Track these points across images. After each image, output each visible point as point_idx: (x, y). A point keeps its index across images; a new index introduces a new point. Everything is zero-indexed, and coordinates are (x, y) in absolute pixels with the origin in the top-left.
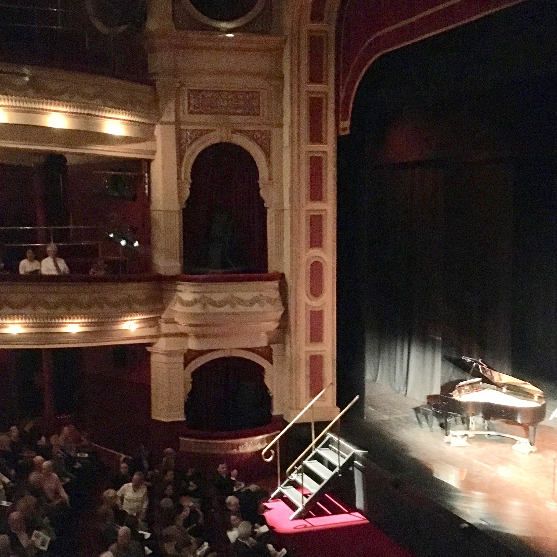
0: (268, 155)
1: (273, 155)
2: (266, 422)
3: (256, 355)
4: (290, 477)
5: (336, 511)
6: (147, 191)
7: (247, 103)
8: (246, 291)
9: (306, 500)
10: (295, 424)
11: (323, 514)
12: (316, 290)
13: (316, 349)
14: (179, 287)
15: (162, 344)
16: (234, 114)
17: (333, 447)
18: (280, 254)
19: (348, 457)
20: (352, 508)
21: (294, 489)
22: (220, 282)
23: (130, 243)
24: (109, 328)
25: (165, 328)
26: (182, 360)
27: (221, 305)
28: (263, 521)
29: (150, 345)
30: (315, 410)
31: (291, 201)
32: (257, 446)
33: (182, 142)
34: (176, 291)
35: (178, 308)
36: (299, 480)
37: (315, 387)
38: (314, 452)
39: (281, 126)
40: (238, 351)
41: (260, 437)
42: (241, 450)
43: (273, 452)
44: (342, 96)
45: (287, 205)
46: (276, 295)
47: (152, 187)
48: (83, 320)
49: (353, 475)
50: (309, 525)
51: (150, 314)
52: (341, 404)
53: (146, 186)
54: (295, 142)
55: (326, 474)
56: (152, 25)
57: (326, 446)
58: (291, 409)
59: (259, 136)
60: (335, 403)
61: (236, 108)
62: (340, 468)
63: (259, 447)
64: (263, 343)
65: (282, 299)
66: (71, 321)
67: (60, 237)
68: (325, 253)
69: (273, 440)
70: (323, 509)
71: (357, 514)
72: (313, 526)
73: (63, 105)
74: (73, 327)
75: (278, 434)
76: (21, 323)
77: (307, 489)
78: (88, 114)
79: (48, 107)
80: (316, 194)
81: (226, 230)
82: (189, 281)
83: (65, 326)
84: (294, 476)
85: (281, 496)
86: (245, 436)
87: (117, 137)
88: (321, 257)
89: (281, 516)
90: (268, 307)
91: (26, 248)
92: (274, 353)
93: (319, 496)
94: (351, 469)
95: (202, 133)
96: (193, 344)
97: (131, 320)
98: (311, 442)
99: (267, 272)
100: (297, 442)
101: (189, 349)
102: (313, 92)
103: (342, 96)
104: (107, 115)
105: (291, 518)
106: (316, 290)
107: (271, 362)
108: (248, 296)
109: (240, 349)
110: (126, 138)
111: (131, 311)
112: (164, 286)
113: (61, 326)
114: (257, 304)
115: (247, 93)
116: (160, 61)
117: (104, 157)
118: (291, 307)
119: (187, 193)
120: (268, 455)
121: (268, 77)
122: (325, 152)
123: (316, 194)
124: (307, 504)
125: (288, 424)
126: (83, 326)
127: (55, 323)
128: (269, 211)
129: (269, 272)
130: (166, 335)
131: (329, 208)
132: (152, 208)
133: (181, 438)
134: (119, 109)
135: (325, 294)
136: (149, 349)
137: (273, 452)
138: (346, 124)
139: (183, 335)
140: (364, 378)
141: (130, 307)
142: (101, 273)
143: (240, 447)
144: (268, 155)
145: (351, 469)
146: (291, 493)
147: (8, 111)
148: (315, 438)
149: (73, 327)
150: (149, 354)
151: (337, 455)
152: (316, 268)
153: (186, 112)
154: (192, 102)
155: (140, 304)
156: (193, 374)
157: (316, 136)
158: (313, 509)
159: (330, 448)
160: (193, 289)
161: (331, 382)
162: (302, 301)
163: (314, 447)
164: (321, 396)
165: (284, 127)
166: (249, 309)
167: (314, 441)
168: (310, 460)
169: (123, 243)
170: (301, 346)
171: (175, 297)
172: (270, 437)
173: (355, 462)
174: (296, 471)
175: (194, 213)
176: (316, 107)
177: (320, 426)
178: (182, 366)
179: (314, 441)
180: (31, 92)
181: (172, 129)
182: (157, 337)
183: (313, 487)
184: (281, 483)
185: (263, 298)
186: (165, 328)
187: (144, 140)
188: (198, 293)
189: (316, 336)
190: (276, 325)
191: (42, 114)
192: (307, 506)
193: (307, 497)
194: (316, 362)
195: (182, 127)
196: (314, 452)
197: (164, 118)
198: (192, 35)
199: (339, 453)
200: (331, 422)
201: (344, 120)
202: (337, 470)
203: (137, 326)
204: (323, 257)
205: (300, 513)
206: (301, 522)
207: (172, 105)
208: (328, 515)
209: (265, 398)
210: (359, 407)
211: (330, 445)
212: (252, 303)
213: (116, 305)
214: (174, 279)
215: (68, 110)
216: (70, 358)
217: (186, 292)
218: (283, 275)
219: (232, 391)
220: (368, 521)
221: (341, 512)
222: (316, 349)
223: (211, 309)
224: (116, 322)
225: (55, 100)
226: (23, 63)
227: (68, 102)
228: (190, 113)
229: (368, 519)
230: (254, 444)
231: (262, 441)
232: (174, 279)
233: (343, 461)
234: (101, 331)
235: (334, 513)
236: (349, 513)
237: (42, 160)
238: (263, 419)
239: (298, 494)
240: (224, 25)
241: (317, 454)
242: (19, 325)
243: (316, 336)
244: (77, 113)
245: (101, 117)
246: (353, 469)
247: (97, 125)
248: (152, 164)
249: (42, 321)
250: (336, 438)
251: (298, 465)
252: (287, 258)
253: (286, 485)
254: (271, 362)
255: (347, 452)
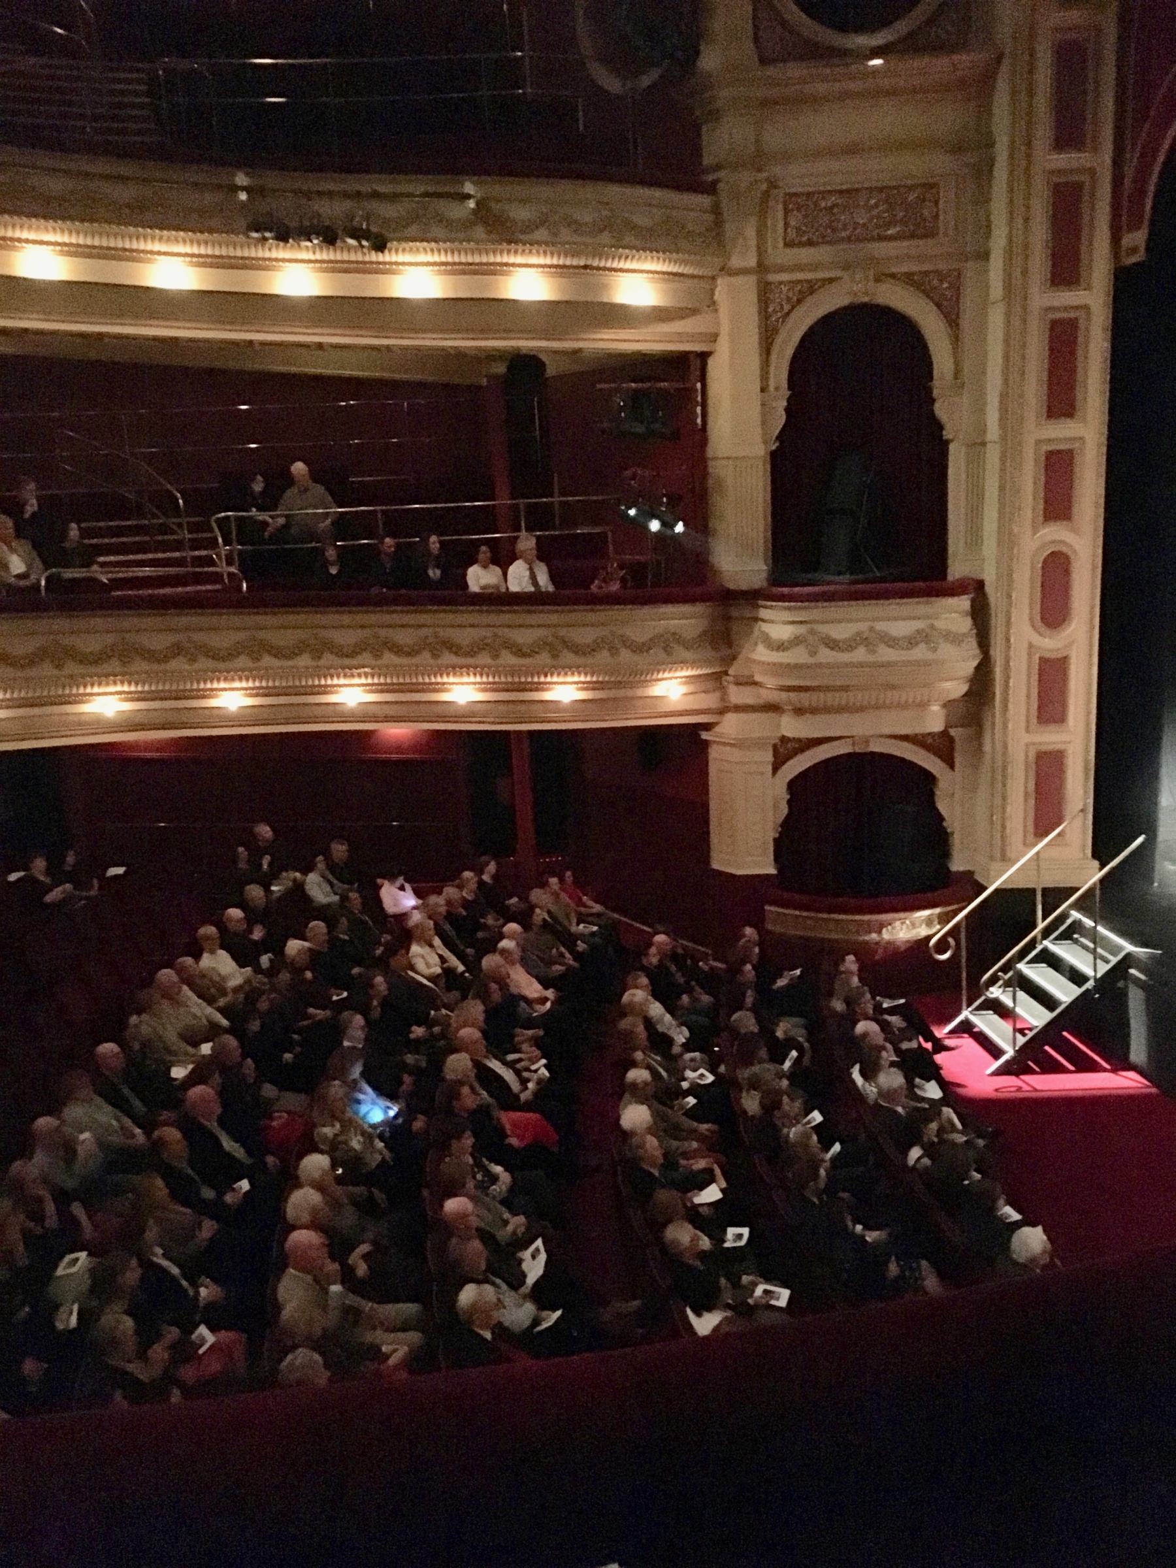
0: (953, 320)
1: (966, 321)
2: (936, 882)
3: (922, 752)
4: (988, 994)
5: (1085, 1066)
6: (699, 421)
7: (909, 210)
8: (899, 619)
9: (1021, 1040)
10: (997, 891)
11: (1058, 1069)
12: (1053, 611)
13: (1050, 738)
14: (764, 613)
15: (730, 726)
16: (881, 238)
17: (1083, 940)
18: (975, 538)
19: (1114, 960)
20: (1121, 1063)
21: (996, 1017)
22: (633, 603)
23: (667, 525)
24: (630, 693)
25: (737, 695)
26: (769, 756)
27: (850, 645)
28: (934, 1073)
29: (707, 727)
30: (1043, 865)
31: (1003, 420)
32: (918, 930)
33: (770, 310)
34: (756, 619)
35: (762, 654)
36: (1007, 1000)
37: (1046, 818)
38: (1039, 948)
39: (985, 256)
40: (882, 740)
41: (927, 913)
42: (886, 935)
43: (951, 940)
44: (1129, 172)
45: (993, 431)
46: (965, 625)
47: (711, 410)
48: (126, 688)
49: (1126, 995)
50: (1026, 1088)
51: (701, 667)
52: (1101, 853)
53: (699, 409)
54: (1014, 293)
55: (1065, 992)
56: (710, 61)
57: (1067, 936)
58: (992, 858)
59: (935, 282)
60: (1089, 852)
61: (888, 225)
62: (1096, 980)
63: (923, 932)
64: (934, 721)
65: (978, 635)
66: (561, 679)
67: (538, 519)
68: (1076, 531)
69: (953, 918)
70: (1092, 1059)
71: (1132, 1074)
72: (1036, 1090)
73: (538, 252)
74: (565, 691)
75: (964, 908)
76: (475, 683)
77: (1024, 1020)
78: (586, 267)
79: (512, 259)
80: (1061, 402)
81: (866, 491)
82: (782, 598)
83: (336, 692)
84: (995, 992)
85: (966, 1028)
86: (895, 910)
87: (637, 308)
88: (1061, 542)
89: (971, 1069)
90: (947, 651)
91: (476, 544)
92: (958, 745)
93: (1049, 1033)
94: (1121, 984)
95: (811, 288)
96: (791, 727)
97: (671, 678)
98: (1034, 926)
99: (944, 577)
100: (1005, 924)
101: (783, 737)
102: (1060, 172)
103: (1129, 172)
104: (622, 265)
105: (989, 1071)
106: (1053, 611)
107: (952, 766)
108: (901, 629)
109: (881, 736)
110: (655, 309)
111: (671, 661)
112: (735, 613)
113: (543, 690)
114: (922, 646)
115: (911, 188)
116: (725, 139)
117: (622, 356)
118: (997, 653)
119: (779, 419)
120: (942, 946)
121: (957, 149)
122: (1086, 308)
123: (1061, 402)
124: (1021, 1048)
125: (985, 888)
126: (251, 696)
127: (532, 683)
128: (952, 447)
129: (950, 578)
130: (738, 709)
131: (1088, 433)
132: (710, 453)
133: (767, 907)
134: (644, 250)
135: (1073, 626)
136: (705, 735)
137: (951, 940)
138: (1137, 238)
139: (773, 708)
140: (1156, 804)
141: (555, 657)
142: (615, 587)
143: (884, 930)
144: (953, 320)
145: (1121, 984)
146: (987, 1023)
147: (440, 273)
148: (1044, 919)
149: (565, 691)
150: (706, 744)
151: (1091, 957)
152: (1056, 568)
153: (781, 244)
154: (793, 223)
155: (687, 646)
156: (791, 785)
157: (1065, 269)
158: (1033, 1055)
159: (1076, 941)
160: (786, 616)
161: (1081, 807)
162: (1022, 638)
163: (1039, 937)
164: (1059, 835)
165: (993, 256)
166: (844, 657)
167: (1041, 926)
168: (1028, 963)
169: (655, 526)
170: (1016, 732)
171: (756, 633)
172: (947, 914)
173: (1132, 971)
174: (1001, 982)
175: (794, 464)
176: (1067, 204)
177: (1055, 896)
178: (770, 767)
179: (1041, 926)
180: (480, 232)
181: (748, 286)
182: (722, 712)
183: (1035, 1016)
184: (969, 1006)
185: (935, 633)
186: (737, 695)
187: (694, 312)
188: (801, 622)
189: (1050, 708)
190: (964, 688)
191: (502, 273)
192: (1022, 1052)
193: (1024, 1035)
194: (1048, 767)
195: (772, 277)
196: (1039, 948)
197: (736, 262)
198: (795, 70)
199: (1094, 952)
200: (1078, 889)
201: (1134, 227)
202: (1090, 984)
203: (684, 689)
204: (1068, 540)
205: (1007, 1062)
206: (1009, 1082)
207: (751, 232)
208: (1067, 1071)
209: (937, 839)
210: (1143, 860)
211: (1075, 936)
212: (911, 642)
213: (641, 648)
214: (753, 597)
215: (548, 261)
216: (559, 752)
217: (778, 623)
218: (980, 585)
219: (871, 819)
220: (1154, 1090)
221: (1093, 1067)
222: (1050, 738)
223: (826, 655)
224: (639, 682)
225: (516, 243)
226: (457, 170)
227: (551, 244)
228: (788, 244)
229: (1158, 1087)
230: (913, 925)
231: (929, 922)
232: (753, 597)
233: (1103, 968)
234: (615, 699)
235: (1044, 1071)
236: (1114, 1070)
237: (501, 369)
238: (929, 874)
239: (1006, 1027)
240: (862, 41)
241: (1045, 950)
242: (472, 686)
243: (1050, 708)
244: (564, 267)
245: (615, 270)
246: (1127, 987)
247: (605, 287)
248: (711, 362)
249: (510, 680)
250: (1089, 923)
251: (1005, 969)
252: (990, 546)
253: (978, 1008)
254: (952, 766)
255: (1115, 949)
